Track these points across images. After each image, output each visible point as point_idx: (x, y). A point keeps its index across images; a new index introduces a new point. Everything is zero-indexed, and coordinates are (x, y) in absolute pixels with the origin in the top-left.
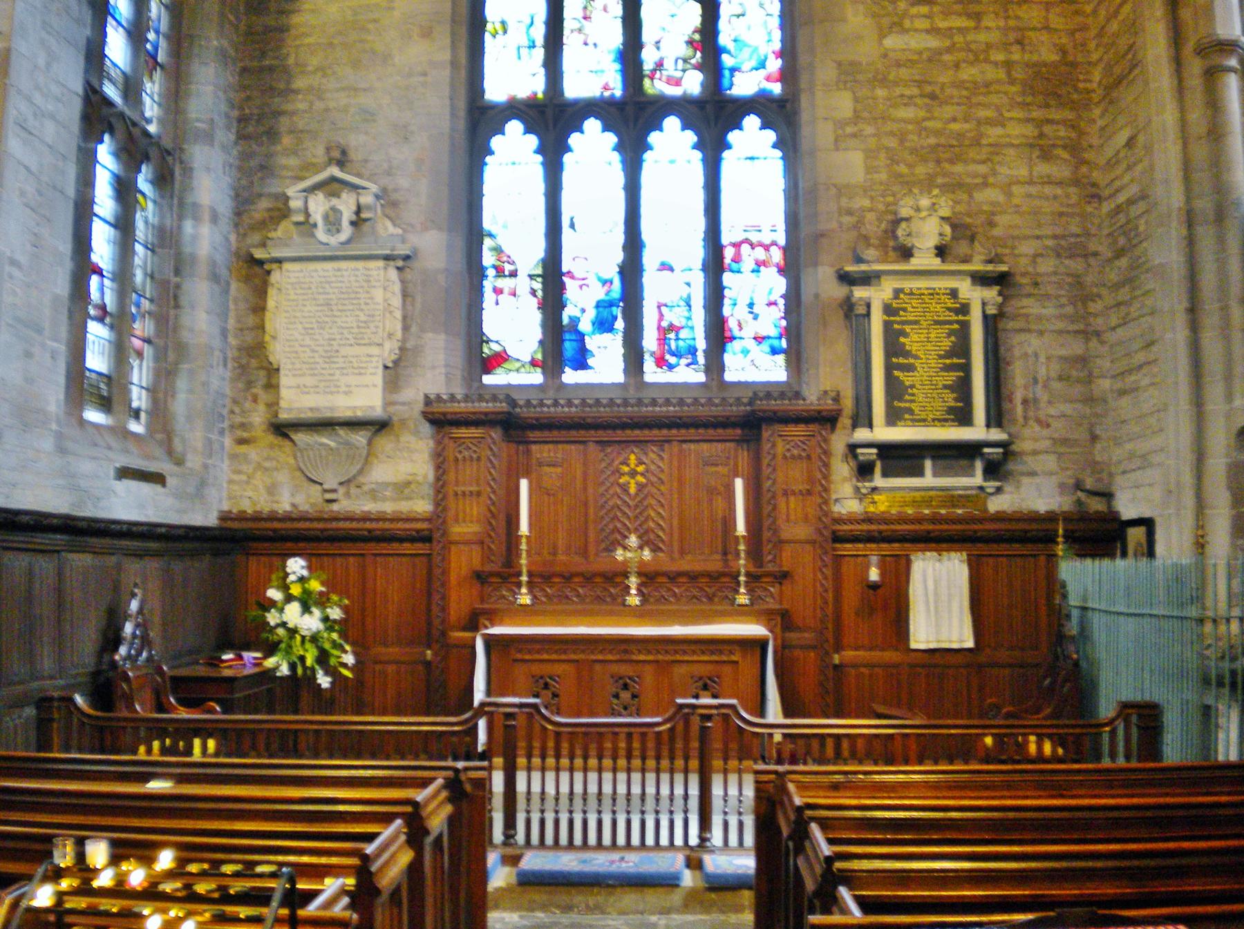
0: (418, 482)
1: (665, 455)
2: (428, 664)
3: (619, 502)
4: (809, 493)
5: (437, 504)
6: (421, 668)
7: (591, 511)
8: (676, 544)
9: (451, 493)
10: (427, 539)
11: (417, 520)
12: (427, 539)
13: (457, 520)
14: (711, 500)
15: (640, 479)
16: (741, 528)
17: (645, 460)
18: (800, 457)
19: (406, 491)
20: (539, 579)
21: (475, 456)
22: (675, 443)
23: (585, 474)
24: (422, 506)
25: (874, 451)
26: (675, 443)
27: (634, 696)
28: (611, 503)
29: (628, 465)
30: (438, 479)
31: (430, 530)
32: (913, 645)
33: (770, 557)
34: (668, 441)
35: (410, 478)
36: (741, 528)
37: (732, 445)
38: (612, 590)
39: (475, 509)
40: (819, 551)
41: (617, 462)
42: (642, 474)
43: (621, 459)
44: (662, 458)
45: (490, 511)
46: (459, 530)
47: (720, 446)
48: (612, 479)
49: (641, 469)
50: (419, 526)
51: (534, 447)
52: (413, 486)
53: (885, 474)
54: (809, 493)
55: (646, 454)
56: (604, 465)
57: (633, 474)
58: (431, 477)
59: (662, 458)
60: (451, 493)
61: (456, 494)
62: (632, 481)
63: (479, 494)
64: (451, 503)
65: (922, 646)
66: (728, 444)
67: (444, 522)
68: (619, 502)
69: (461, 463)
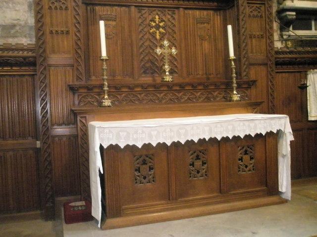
0: (20, 25)
1: (176, 17)
2: (37, 151)
3: (151, 44)
4: (262, 37)
5: (38, 39)
6: (31, 152)
7: (135, 49)
8: (184, 69)
9: (48, 32)
10: (34, 64)
11: (23, 50)
12: (33, 64)
13: (53, 52)
14: (202, 44)
15: (161, 30)
16: (232, 54)
17: (164, 19)
18: (257, 16)
19: (13, 31)
20: (115, 90)
21: (64, 7)
22: (181, 9)
23: (130, 26)
24: (26, 41)
25: (294, 13)
26: (181, 9)
27: (204, 163)
28: (146, 44)
29: (155, 22)
30: (38, 21)
31: (35, 57)
32: (310, 119)
33: (245, 73)
34: (178, 8)
35: (15, 22)
36: (232, 54)
37: (212, 12)
38: (158, 95)
39: (66, 43)
40: (269, 69)
41: (148, 21)
42: (163, 28)
43: (150, 17)
44: (174, 19)
45: (77, 44)
46: (54, 59)
47: (205, 12)
48: (146, 30)
49: (161, 24)
50: (25, 54)
51: (97, 8)
52: (18, 28)
53: (294, 29)
54: (262, 37)
55: (164, 15)
56: (140, 21)
57: (158, 27)
58: (32, 21)
59: (174, 19)
60: (48, 32)
61: (51, 32)
62: (158, 32)
63: (68, 32)
64: (48, 37)
65: (313, 119)
66: (209, 11)
67: (44, 51)
68: (151, 44)
69: (54, 11)
